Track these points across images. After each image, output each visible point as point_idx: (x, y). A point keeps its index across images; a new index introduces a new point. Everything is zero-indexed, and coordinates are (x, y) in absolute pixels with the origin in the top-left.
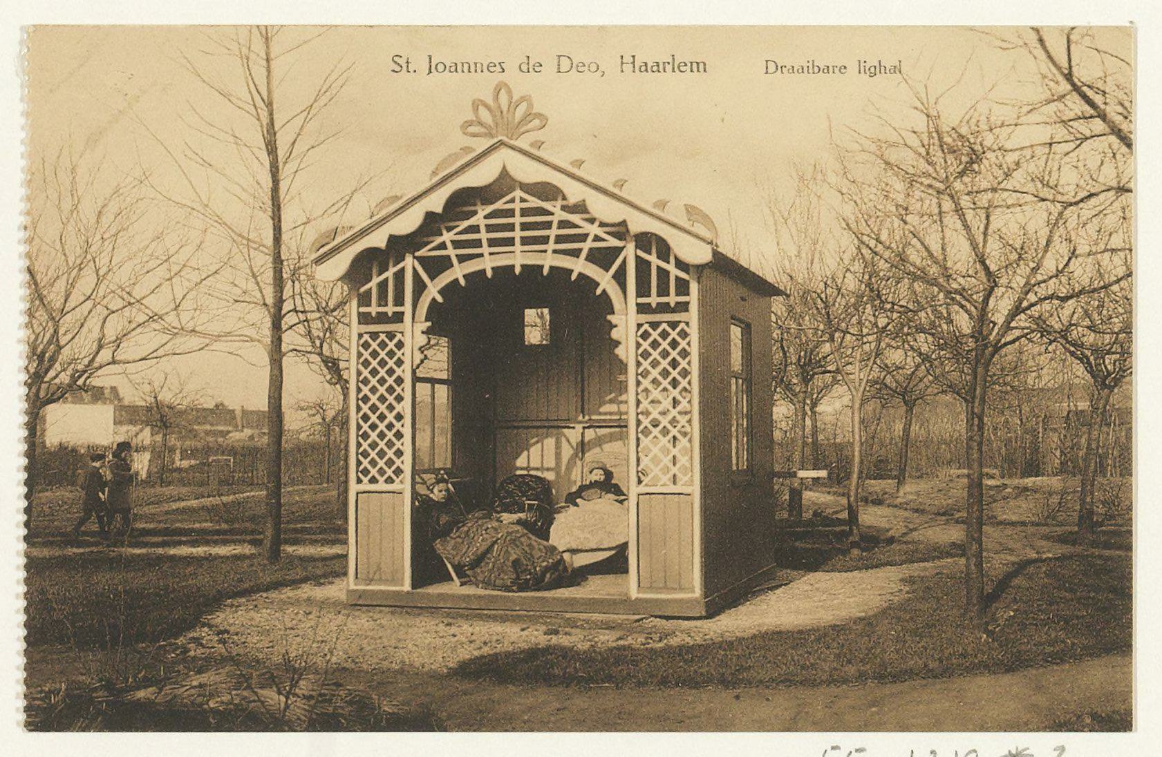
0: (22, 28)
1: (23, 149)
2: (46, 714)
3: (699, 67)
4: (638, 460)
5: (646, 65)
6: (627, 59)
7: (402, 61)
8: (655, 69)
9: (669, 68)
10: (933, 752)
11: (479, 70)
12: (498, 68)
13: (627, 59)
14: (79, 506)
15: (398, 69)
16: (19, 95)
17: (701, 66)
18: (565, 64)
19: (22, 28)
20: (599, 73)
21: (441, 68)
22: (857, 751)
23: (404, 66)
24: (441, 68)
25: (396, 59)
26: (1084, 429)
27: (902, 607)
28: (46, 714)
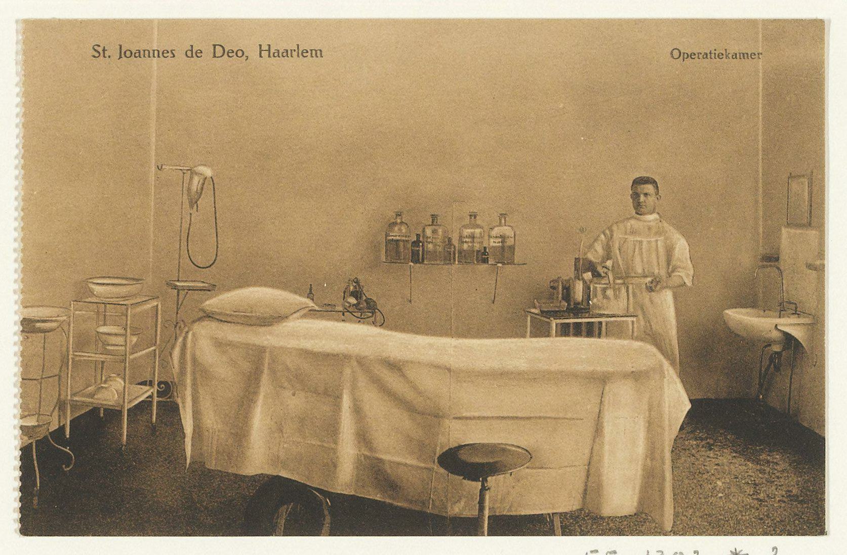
0: (17, 21)
3: (597, 551)
4: (125, 369)
5: (287, 51)
6: (265, 47)
8: (285, 54)
9: (295, 54)
10: (695, 552)
11: (147, 55)
12: (170, 54)
13: (265, 47)
15: (97, 55)
16: (14, 50)
19: (17, 21)
20: (244, 57)
21: (128, 54)
22: (592, 552)
23: (101, 52)
24: (128, 54)
25: (96, 47)
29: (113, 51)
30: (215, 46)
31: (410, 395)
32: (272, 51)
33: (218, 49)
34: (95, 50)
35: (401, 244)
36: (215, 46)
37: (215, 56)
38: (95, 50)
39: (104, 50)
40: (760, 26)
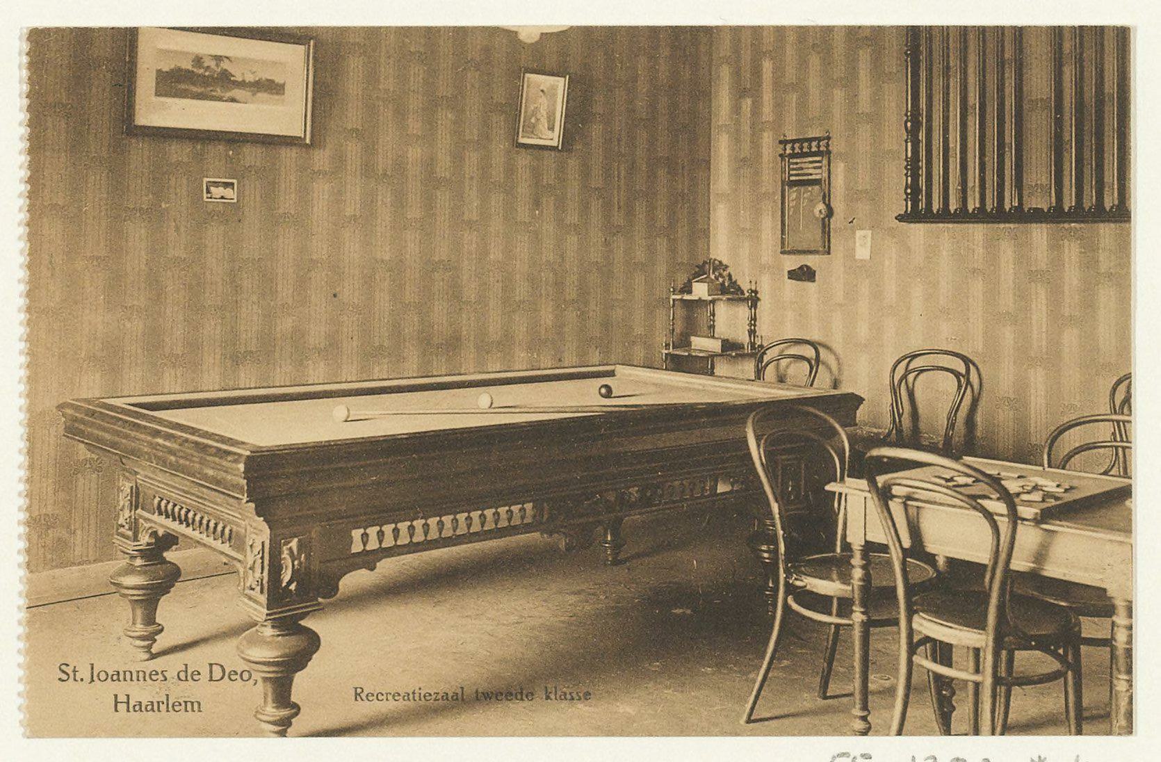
1: (20, 701)
2: (40, 40)
6: (122, 698)
7: (69, 670)
8: (137, 708)
9: (163, 707)
12: (160, 677)
13: (122, 698)
14: (1098, 205)
15: (65, 677)
17: (196, 706)
18: (217, 673)
21: (103, 676)
24: (103, 676)
25: (64, 667)
26: (859, 513)
27: (523, 45)
28: (40, 40)
29: (84, 673)
30: (211, 665)
31: (401, 704)
32: (132, 703)
33: (217, 670)
34: (64, 672)
35: (1120, 450)
36: (211, 665)
37: (211, 680)
38: (64, 672)
39: (75, 671)
40: (1039, 82)
